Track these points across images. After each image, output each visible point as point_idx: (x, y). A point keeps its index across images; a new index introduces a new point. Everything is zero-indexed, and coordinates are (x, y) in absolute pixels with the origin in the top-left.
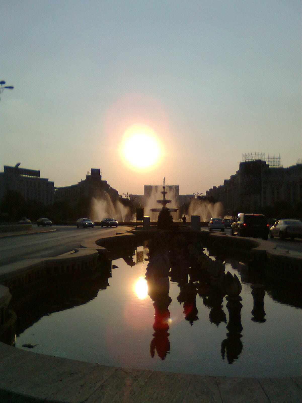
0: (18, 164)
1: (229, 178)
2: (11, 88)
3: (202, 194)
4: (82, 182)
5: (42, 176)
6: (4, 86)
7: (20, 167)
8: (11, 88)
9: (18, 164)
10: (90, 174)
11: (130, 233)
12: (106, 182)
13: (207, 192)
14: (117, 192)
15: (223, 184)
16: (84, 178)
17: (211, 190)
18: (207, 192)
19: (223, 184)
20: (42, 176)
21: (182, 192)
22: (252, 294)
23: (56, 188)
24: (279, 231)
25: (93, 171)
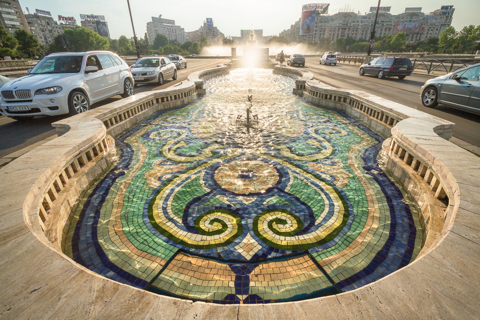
1: (294, 24)
5: (176, 24)
15: (290, 28)
21: (265, 34)
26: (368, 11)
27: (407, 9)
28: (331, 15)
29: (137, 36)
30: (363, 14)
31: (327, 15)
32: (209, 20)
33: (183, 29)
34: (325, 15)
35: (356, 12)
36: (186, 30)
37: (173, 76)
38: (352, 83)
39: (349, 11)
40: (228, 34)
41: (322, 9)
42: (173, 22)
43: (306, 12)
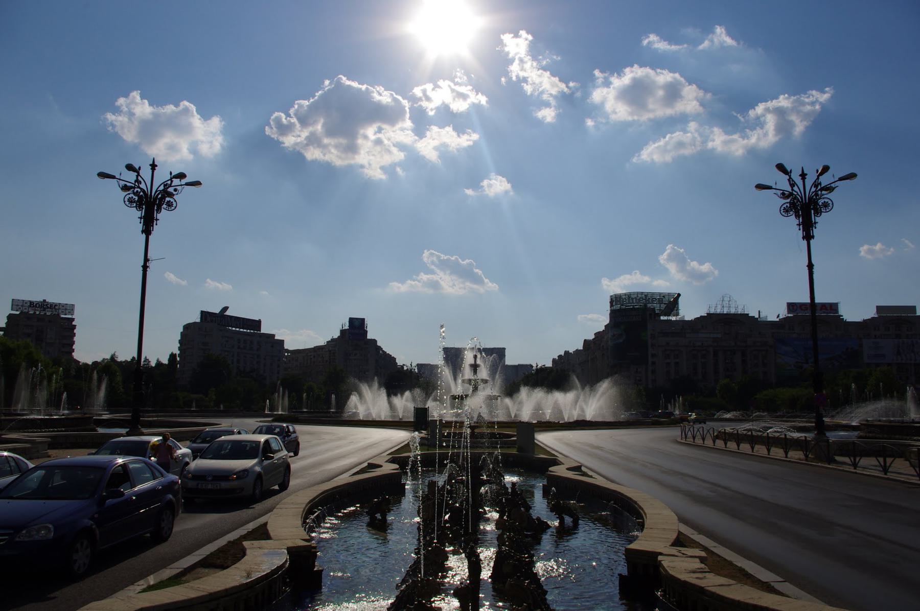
0: (225, 309)
1: (591, 337)
2: (197, 183)
3: (826, 169)
4: (333, 340)
5: (264, 330)
6: (184, 181)
7: (228, 313)
8: (197, 183)
9: (225, 309)
10: (347, 327)
11: (316, 488)
12: (375, 341)
13: (554, 360)
14: (395, 359)
15: (581, 348)
16: (336, 334)
17: (560, 356)
18: (554, 360)
19: (581, 348)
20: (264, 330)
21: (511, 359)
22: (526, 365)
23: (287, 351)
24: (598, 395)
25: (351, 320)
26: (783, 313)
27: (879, 309)
28: (687, 319)
29: (805, 242)
30: (772, 318)
31: (678, 318)
32: (357, 323)
33: (282, 342)
34: (674, 318)
35: (753, 313)
36: (288, 346)
37: (280, 481)
38: (361, 464)
39: (733, 311)
40: (406, 356)
41: (663, 306)
42: (256, 324)
43: (620, 310)
